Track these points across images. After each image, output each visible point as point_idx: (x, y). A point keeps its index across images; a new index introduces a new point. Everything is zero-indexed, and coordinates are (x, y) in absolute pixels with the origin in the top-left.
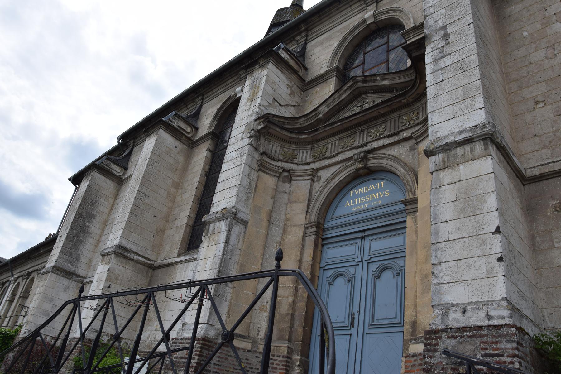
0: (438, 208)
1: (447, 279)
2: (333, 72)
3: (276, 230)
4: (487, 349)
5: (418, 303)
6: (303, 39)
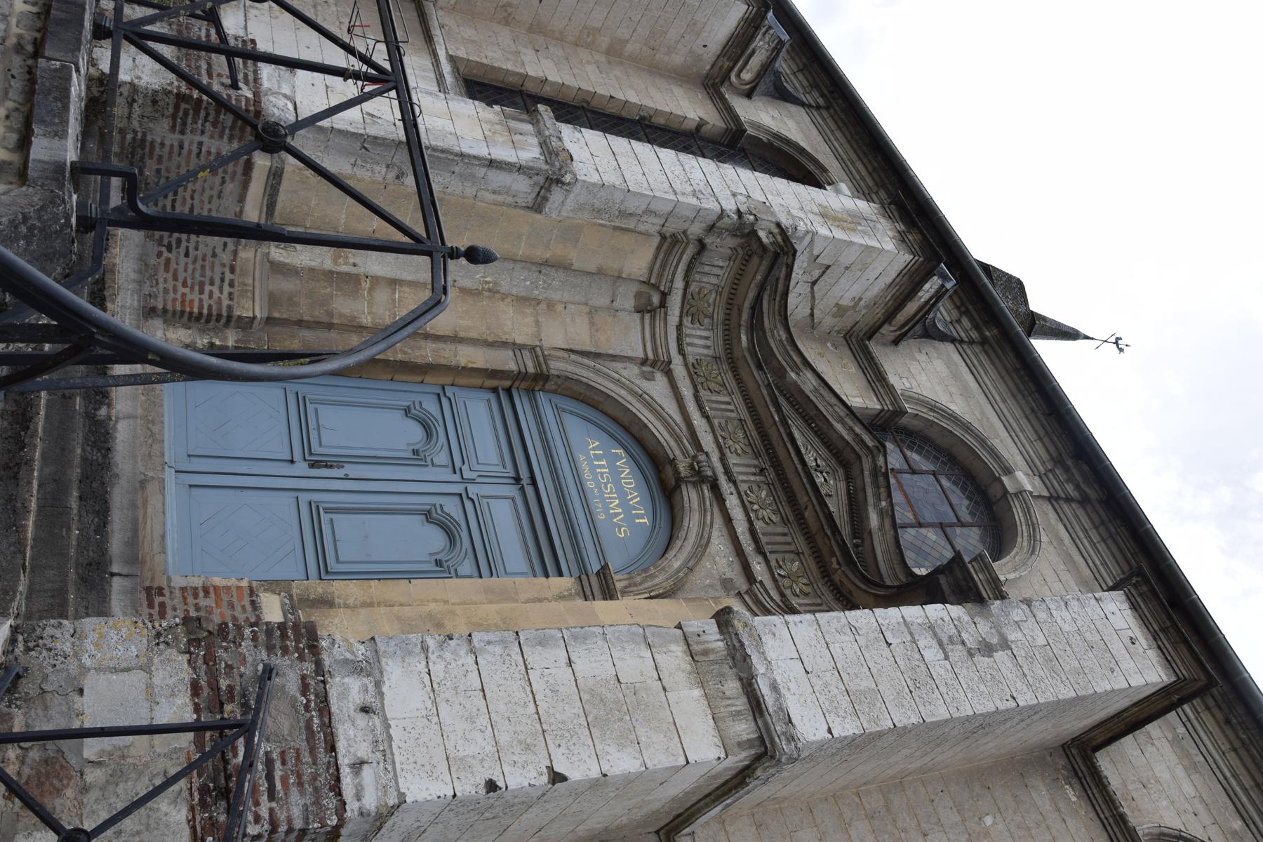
0: (600, 643)
1: (438, 669)
2: (892, 404)
3: (525, 280)
4: (284, 763)
5: (376, 609)
6: (963, 335)
